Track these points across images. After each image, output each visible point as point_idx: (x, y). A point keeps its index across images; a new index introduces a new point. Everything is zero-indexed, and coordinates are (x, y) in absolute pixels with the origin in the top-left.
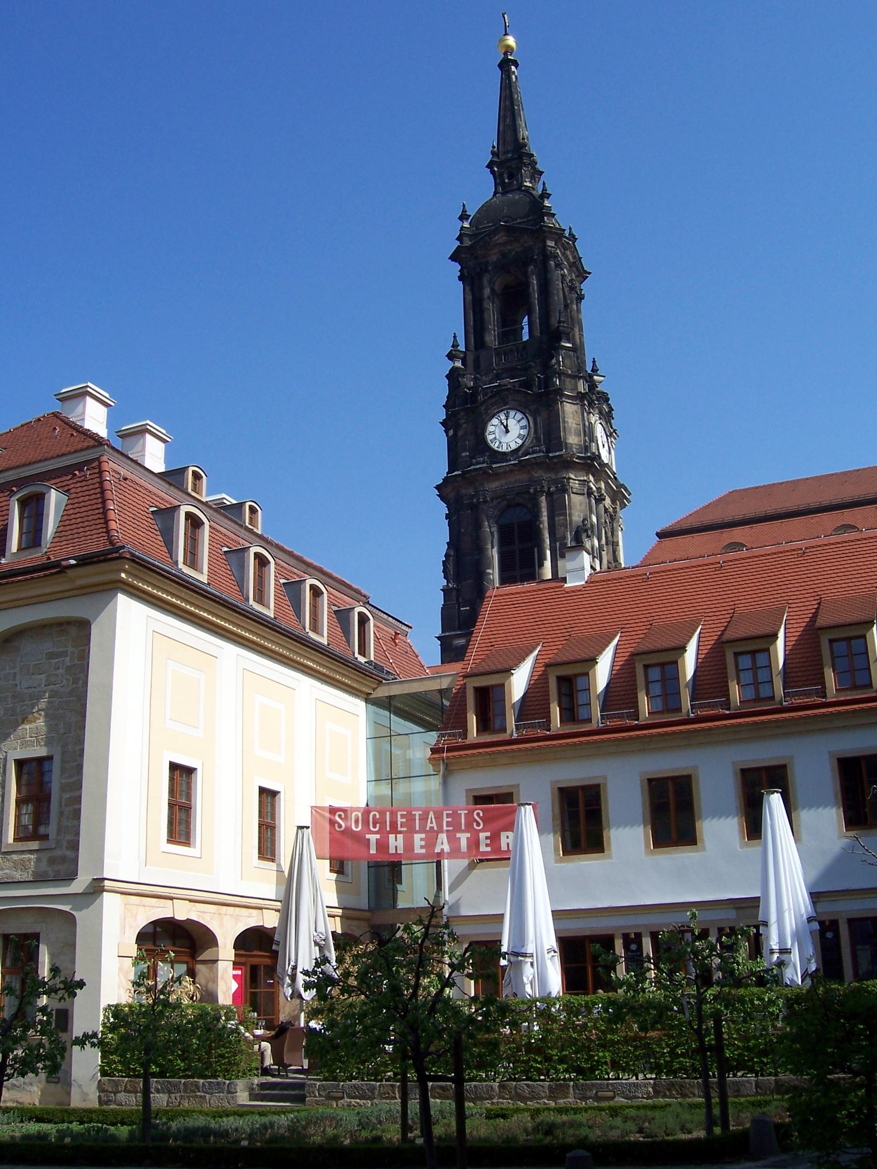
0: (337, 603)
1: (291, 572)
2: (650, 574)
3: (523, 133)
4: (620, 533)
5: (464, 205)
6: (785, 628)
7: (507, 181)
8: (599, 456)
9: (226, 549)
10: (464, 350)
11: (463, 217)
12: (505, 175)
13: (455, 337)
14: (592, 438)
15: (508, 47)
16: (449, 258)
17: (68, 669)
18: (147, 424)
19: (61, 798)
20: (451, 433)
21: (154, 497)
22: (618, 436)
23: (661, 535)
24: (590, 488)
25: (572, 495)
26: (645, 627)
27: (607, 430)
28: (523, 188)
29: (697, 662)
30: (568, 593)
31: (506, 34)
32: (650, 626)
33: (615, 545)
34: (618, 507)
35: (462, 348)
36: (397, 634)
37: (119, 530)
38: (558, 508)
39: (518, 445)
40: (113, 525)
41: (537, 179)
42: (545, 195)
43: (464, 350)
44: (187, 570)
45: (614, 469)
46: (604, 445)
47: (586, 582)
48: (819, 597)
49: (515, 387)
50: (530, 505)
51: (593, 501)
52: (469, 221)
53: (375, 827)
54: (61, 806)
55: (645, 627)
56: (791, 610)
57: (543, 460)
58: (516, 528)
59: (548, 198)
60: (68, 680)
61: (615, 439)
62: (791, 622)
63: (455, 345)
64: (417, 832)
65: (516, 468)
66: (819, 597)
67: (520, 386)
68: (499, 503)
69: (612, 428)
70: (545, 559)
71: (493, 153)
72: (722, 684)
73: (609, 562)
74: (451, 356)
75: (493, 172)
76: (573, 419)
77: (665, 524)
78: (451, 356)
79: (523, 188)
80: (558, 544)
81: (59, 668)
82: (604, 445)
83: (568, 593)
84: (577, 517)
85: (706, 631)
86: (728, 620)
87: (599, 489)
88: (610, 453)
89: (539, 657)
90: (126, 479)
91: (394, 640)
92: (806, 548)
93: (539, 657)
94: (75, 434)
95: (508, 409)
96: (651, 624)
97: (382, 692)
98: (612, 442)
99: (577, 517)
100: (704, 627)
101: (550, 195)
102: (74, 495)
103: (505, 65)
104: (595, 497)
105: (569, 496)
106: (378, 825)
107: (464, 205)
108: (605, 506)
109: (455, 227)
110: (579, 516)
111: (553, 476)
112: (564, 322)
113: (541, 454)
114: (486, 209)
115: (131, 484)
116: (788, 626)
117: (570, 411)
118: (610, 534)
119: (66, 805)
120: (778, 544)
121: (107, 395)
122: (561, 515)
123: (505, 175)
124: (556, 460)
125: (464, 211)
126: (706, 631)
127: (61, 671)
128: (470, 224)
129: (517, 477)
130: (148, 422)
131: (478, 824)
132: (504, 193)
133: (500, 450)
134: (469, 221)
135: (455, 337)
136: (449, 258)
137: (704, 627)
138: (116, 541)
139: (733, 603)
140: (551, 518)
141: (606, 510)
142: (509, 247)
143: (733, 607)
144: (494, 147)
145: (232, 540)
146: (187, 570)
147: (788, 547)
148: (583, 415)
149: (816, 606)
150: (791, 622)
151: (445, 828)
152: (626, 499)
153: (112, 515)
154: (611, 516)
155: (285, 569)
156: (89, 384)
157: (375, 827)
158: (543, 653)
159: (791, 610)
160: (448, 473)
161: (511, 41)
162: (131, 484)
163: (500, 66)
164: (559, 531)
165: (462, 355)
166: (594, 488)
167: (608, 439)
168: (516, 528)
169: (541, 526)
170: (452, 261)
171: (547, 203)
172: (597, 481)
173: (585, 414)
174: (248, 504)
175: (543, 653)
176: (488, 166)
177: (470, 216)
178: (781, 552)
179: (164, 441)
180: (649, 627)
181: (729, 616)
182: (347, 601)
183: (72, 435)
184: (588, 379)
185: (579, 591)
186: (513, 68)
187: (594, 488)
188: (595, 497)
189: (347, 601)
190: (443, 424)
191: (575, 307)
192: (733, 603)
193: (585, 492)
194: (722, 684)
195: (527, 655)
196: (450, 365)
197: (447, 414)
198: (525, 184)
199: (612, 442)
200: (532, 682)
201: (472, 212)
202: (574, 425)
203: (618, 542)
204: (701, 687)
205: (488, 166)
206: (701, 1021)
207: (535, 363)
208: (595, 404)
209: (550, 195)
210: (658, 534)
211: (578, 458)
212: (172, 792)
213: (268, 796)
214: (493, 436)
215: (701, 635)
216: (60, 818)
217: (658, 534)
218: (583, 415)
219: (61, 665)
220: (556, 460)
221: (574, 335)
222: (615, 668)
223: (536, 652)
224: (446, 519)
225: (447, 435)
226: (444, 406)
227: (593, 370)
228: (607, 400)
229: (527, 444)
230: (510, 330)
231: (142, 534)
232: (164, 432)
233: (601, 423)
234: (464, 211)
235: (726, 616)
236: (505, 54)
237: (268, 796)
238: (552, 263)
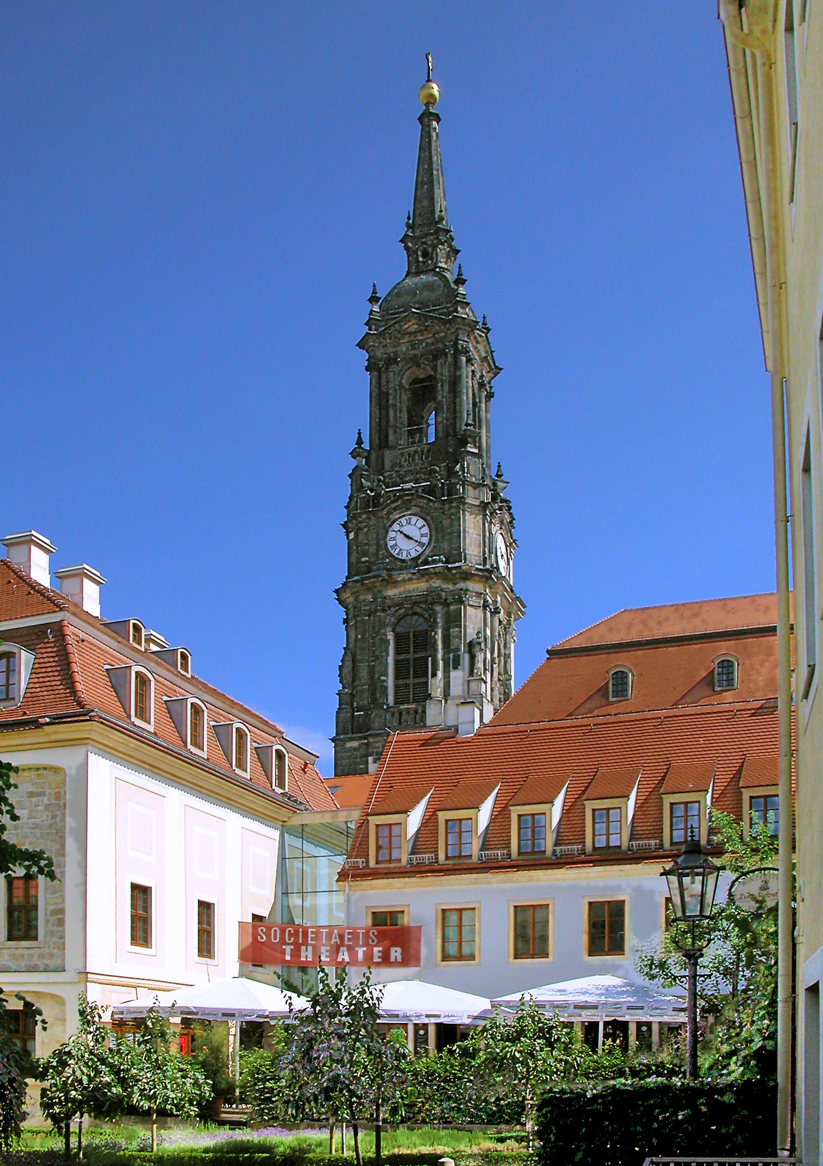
0: (256, 740)
1: (218, 714)
2: (531, 731)
3: (440, 203)
4: (512, 645)
5: (374, 286)
6: (638, 788)
7: (421, 259)
8: (498, 568)
9: (165, 698)
10: (368, 449)
11: (373, 299)
12: (419, 253)
13: (359, 434)
14: (493, 550)
15: (432, 96)
16: (357, 345)
17: (47, 807)
18: (84, 568)
19: (46, 909)
20: (352, 536)
21: (106, 654)
22: (518, 547)
23: (553, 654)
24: (485, 601)
25: (468, 607)
26: (522, 779)
27: (507, 540)
28: (437, 270)
29: (563, 810)
30: (459, 743)
31: (429, 81)
32: (523, 783)
33: (507, 657)
34: (512, 619)
35: (366, 446)
36: (306, 764)
37: (84, 691)
38: (454, 620)
39: (418, 553)
40: (79, 687)
41: (453, 259)
42: (460, 281)
43: (368, 449)
44: (138, 722)
45: (511, 583)
46: (502, 556)
47: (475, 735)
48: (668, 763)
49: (417, 491)
50: (427, 615)
51: (488, 614)
52: (379, 303)
53: (290, 939)
54: (46, 915)
55: (522, 779)
56: (644, 772)
57: (441, 571)
58: (411, 636)
59: (463, 284)
60: (47, 816)
61: (515, 549)
62: (643, 783)
63: (360, 442)
64: (324, 945)
65: (414, 577)
66: (668, 763)
67: (423, 491)
68: (396, 611)
69: (512, 538)
70: (438, 670)
71: (409, 227)
72: (581, 833)
73: (499, 674)
74: (354, 454)
75: (407, 248)
76: (474, 529)
77: (558, 642)
78: (354, 454)
79: (437, 270)
80: (452, 655)
81: (38, 806)
82: (502, 556)
83: (459, 743)
84: (471, 634)
85: (572, 786)
86: (592, 777)
87: (495, 602)
88: (508, 564)
89: (431, 800)
90: (83, 641)
91: (303, 770)
92: (665, 718)
93: (431, 800)
94: (32, 592)
95: (410, 515)
96: (527, 777)
97: (296, 820)
98: (511, 552)
99: (471, 634)
100: (571, 782)
101: (466, 281)
102: (40, 656)
103: (427, 117)
104: (491, 609)
105: (465, 608)
106: (292, 938)
107: (374, 286)
108: (499, 619)
109: (364, 310)
110: (474, 629)
111: (451, 587)
112: (471, 425)
113: (441, 564)
114: (397, 291)
115: (88, 645)
116: (640, 787)
117: (471, 524)
118: (502, 647)
119: (52, 915)
120: (642, 711)
121: (48, 542)
122: (456, 626)
123: (419, 253)
124: (454, 571)
125: (374, 292)
126: (572, 786)
127: (40, 808)
128: (380, 308)
129: (416, 586)
130: (85, 566)
131: (373, 941)
132: (418, 273)
133: (400, 557)
134: (379, 303)
135: (359, 434)
136: (357, 345)
137: (571, 782)
138: (85, 703)
139: (597, 763)
140: (446, 630)
141: (500, 622)
142: (420, 338)
143: (597, 766)
144: (409, 218)
145: (170, 688)
146: (138, 722)
147: (649, 715)
148: (484, 525)
149: (665, 771)
150: (643, 783)
151: (346, 943)
152: (521, 611)
153: (78, 677)
154: (505, 628)
155: (214, 712)
156: (33, 532)
157: (290, 939)
158: (434, 796)
159: (644, 772)
160: (347, 578)
161: (435, 89)
162: (88, 645)
163: (420, 119)
164: (454, 643)
165: (365, 454)
166: (490, 601)
167: (507, 550)
168: (411, 636)
169: (436, 637)
170: (360, 348)
171: (462, 290)
172: (494, 594)
173: (487, 525)
174: (179, 651)
175: (434, 796)
176: (402, 241)
177: (380, 298)
178: (643, 720)
179: (98, 583)
180: (525, 779)
181: (593, 774)
182: (266, 739)
183: (30, 593)
184: (492, 487)
185: (469, 742)
186: (434, 124)
187: (490, 601)
188: (491, 609)
189: (266, 739)
190: (345, 525)
191: (483, 406)
192: (597, 763)
193: (481, 605)
194: (581, 833)
195: (422, 798)
196: (354, 463)
197: (348, 516)
198: (440, 265)
199: (511, 552)
200: (424, 821)
201: (382, 294)
202: (475, 536)
203: (510, 654)
204: (563, 834)
205: (402, 241)
206: (123, 1150)
207: (440, 467)
208: (497, 514)
209: (466, 281)
210: (548, 652)
211: (477, 569)
212: (134, 906)
213: (206, 909)
214: (394, 542)
215: (569, 789)
216: (47, 924)
217: (548, 652)
218: (484, 525)
219: (40, 803)
220: (454, 571)
221: (480, 438)
222: (494, 813)
223: (429, 795)
224: (344, 624)
225: (348, 538)
226: (345, 507)
227: (497, 476)
228: (510, 508)
229: (427, 552)
230: (416, 421)
231: (101, 692)
232: (98, 574)
233: (501, 534)
234: (374, 292)
235: (587, 778)
236: (427, 104)
237: (206, 909)
238: (464, 359)
